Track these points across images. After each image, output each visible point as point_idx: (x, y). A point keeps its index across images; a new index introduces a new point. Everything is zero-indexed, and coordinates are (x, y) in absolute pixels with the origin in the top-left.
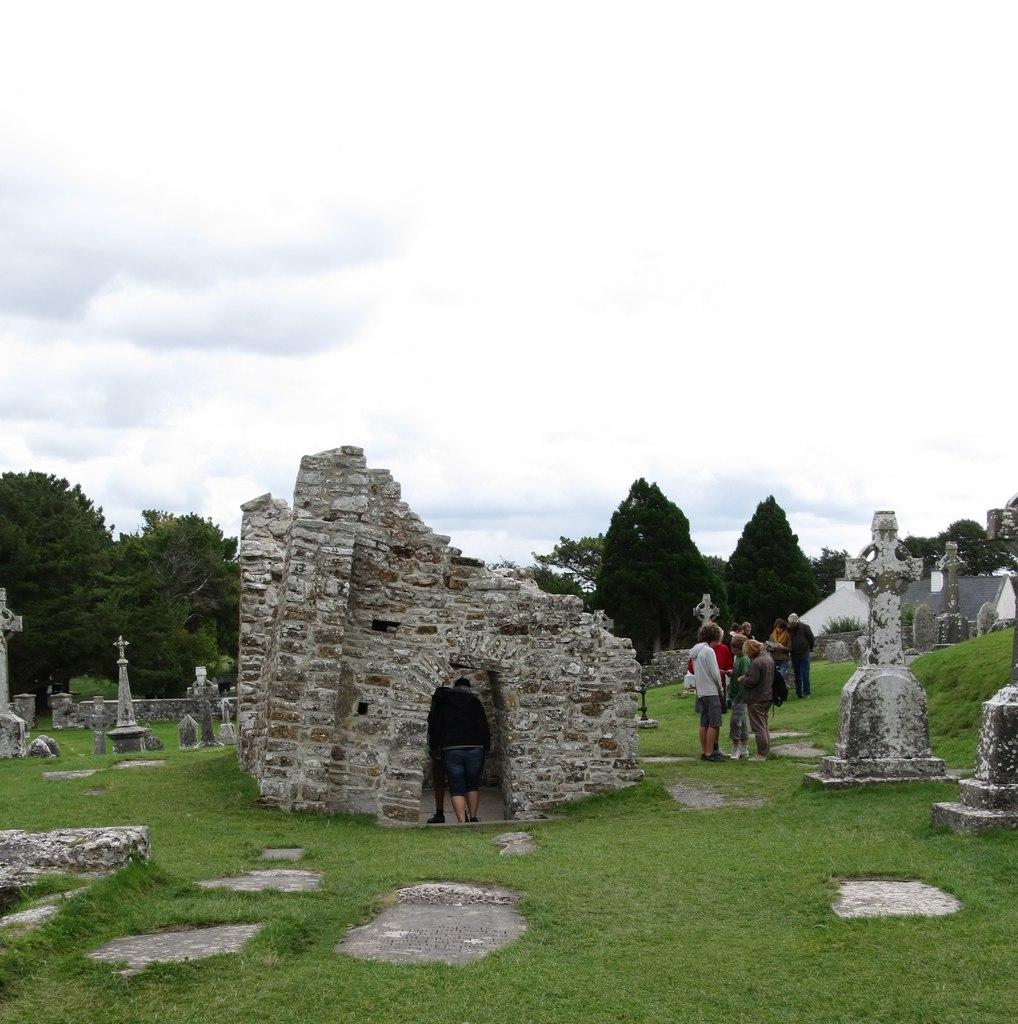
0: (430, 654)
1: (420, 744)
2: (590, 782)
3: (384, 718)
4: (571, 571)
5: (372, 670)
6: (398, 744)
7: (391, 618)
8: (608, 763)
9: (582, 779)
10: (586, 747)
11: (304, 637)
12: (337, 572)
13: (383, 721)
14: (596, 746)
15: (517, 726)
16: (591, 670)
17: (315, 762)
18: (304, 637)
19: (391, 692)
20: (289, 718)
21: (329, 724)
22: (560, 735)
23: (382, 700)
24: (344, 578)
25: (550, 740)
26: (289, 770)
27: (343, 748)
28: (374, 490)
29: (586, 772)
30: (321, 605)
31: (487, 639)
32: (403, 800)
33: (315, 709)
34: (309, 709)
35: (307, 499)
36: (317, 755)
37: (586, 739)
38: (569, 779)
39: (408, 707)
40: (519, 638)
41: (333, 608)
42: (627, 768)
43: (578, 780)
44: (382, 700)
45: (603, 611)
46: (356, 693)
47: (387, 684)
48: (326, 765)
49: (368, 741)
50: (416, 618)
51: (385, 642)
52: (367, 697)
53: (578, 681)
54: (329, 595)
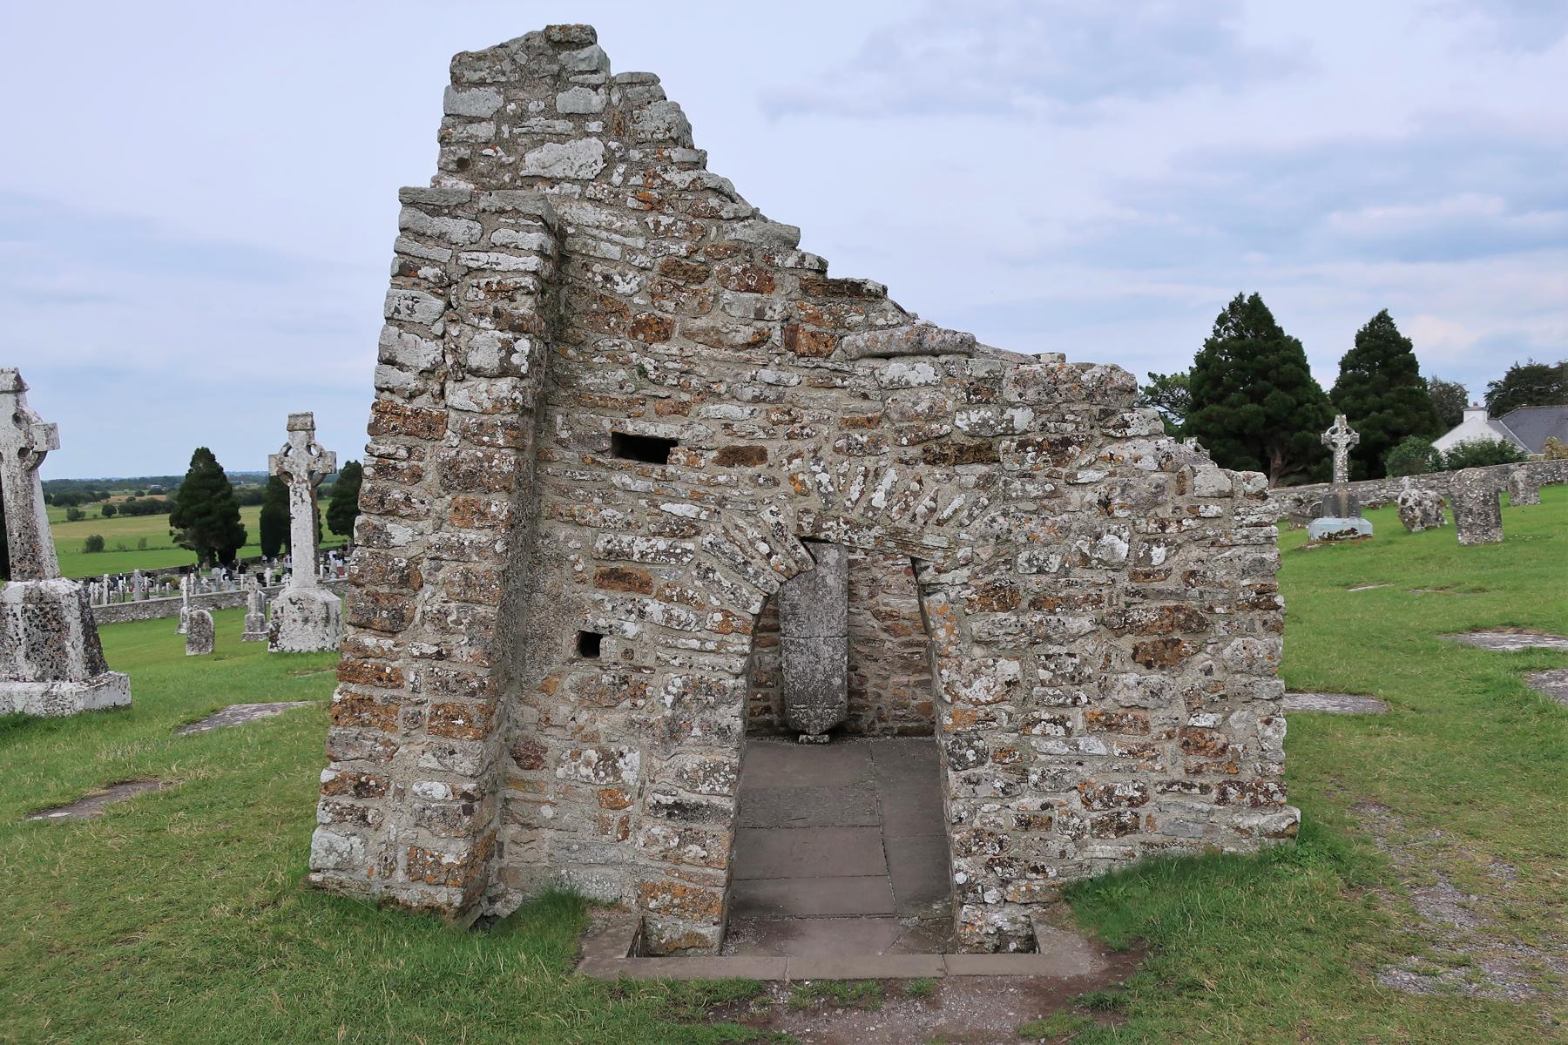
0: (748, 513)
1: (723, 732)
2: (1156, 838)
3: (639, 669)
4: (1164, 410)
5: (610, 553)
6: (674, 732)
7: (660, 430)
8: (1205, 789)
9: (1135, 828)
10: (1145, 747)
11: (417, 476)
12: (497, 314)
13: (635, 677)
14: (1172, 746)
15: (963, 692)
16: (1158, 553)
17: (439, 790)
18: (417, 476)
19: (655, 608)
20: (379, 677)
21: (473, 694)
22: (1077, 720)
23: (631, 628)
24: (513, 328)
25: (1050, 729)
26: (373, 806)
27: (543, 740)
28: (618, 125)
29: (1143, 811)
30: (458, 396)
31: (891, 476)
32: (684, 868)
33: (439, 656)
34: (423, 656)
35: (464, 152)
36: (445, 774)
37: (1146, 728)
38: (1101, 828)
39: (695, 644)
40: (971, 473)
41: (488, 405)
42: (1255, 804)
43: (1122, 829)
44: (631, 628)
45: (1194, 439)
46: (575, 608)
47: (644, 586)
48: (465, 795)
49: (606, 722)
50: (716, 427)
51: (640, 485)
52: (596, 620)
53: (1124, 581)
54: (477, 372)
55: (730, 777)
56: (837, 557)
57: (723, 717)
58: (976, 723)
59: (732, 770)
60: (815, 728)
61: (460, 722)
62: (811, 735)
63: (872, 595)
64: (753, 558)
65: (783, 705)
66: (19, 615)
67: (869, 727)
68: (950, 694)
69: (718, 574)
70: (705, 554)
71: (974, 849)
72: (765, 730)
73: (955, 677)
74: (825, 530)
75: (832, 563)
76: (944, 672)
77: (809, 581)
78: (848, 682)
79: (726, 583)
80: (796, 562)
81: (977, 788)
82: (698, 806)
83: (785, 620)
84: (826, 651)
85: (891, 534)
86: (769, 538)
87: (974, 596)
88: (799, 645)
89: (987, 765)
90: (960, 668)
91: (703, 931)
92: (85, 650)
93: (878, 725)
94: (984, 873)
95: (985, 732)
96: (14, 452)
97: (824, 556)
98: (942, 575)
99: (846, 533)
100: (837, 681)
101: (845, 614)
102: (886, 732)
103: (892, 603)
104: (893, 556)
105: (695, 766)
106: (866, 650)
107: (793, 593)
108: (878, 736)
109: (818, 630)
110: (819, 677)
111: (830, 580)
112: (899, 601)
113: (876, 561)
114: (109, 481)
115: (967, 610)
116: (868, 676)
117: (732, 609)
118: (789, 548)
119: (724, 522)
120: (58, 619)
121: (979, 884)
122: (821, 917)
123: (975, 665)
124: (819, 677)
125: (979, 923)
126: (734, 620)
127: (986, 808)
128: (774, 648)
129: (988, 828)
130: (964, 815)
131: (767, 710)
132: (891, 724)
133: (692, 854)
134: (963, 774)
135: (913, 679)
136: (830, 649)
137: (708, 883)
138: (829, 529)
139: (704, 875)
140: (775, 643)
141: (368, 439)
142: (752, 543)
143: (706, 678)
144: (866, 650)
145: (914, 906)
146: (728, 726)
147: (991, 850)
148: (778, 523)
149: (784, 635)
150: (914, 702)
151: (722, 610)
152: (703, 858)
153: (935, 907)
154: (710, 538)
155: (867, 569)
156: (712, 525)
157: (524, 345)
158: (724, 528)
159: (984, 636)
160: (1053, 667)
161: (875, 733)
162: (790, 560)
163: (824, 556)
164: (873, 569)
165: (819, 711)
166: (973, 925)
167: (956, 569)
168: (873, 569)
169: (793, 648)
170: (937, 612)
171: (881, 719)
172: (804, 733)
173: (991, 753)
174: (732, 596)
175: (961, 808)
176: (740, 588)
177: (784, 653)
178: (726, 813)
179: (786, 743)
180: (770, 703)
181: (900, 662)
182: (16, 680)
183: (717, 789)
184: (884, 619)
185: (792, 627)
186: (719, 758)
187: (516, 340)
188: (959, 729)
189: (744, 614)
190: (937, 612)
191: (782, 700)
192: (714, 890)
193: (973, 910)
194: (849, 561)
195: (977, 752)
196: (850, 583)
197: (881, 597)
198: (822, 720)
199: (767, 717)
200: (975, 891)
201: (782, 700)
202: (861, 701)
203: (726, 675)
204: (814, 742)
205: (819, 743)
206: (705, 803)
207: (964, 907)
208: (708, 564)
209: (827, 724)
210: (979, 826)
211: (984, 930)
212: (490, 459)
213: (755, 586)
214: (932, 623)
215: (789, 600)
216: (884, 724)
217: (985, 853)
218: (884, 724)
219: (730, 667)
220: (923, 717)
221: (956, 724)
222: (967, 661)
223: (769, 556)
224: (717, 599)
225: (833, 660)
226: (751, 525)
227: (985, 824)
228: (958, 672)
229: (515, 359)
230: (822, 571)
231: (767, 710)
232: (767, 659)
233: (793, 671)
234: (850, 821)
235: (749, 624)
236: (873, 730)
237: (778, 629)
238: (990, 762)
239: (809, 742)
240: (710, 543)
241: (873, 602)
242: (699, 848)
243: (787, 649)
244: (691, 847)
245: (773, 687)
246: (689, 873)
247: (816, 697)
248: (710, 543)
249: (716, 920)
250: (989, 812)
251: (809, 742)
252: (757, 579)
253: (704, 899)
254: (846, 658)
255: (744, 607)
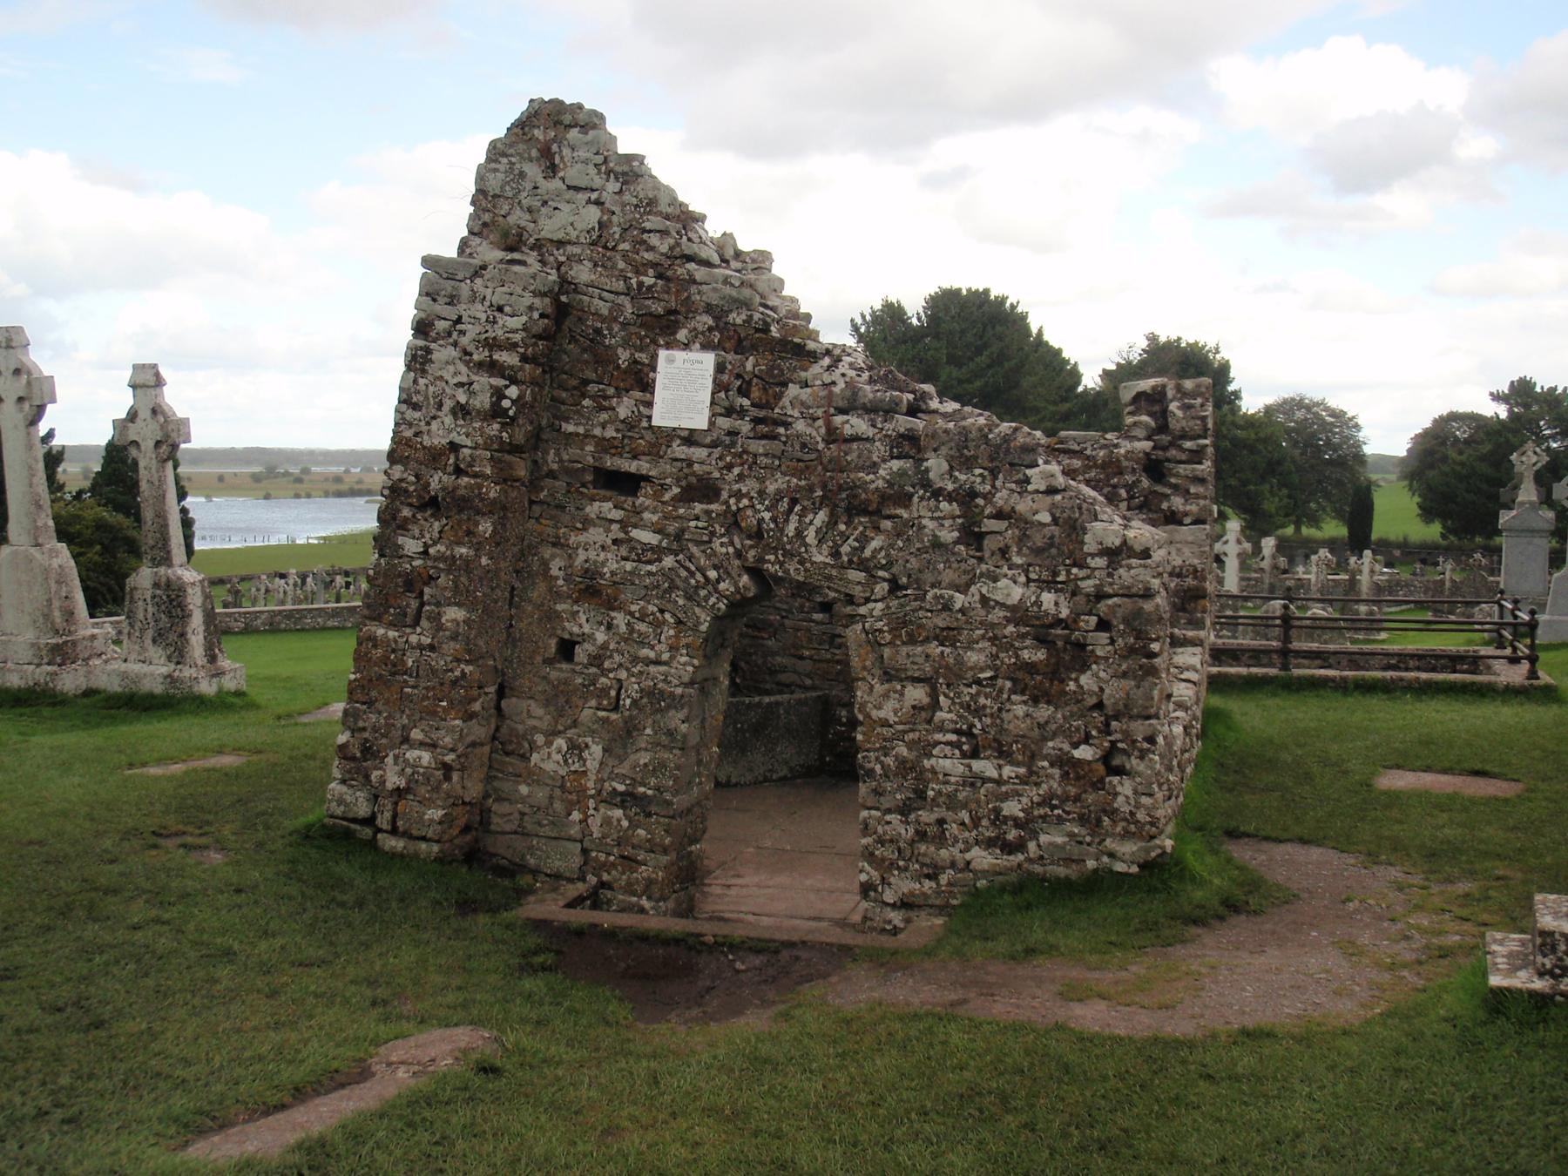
19: (620, 620)
61: (445, 704)
66: (149, 600)
92: (205, 638)
96: (151, 444)
114: (311, 453)
120: (182, 606)
141: (387, 465)
147: (1334, 986)
157: (513, 392)
160: (952, 695)
182: (144, 662)
187: (507, 387)
212: (480, 487)
229: (506, 403)
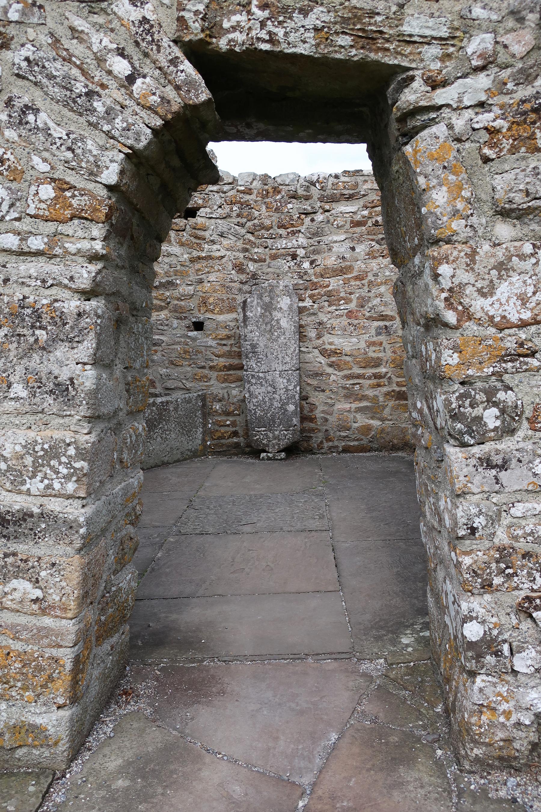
55: (77, 465)
56: (289, 303)
57: (61, 364)
58: (502, 359)
59: (81, 454)
60: (274, 447)
62: (271, 453)
63: (319, 337)
64: (103, 86)
65: (248, 429)
67: (318, 446)
68: (455, 310)
69: (43, 116)
70: (20, 82)
71: (497, 581)
72: (234, 451)
73: (464, 277)
74: (228, 31)
75: (285, 308)
76: (444, 269)
77: (266, 324)
78: (301, 408)
79: (58, 132)
80: (178, 88)
81: (503, 475)
82: (26, 515)
83: (247, 357)
84: (281, 383)
85: (345, 20)
86: (130, 49)
87: (499, 123)
88: (259, 378)
89: (520, 434)
90: (474, 261)
91: (39, 720)
93: (326, 445)
94: (515, 621)
95: (517, 377)
97: (278, 302)
98: (439, 91)
99: (263, 25)
100: (291, 408)
101: (297, 351)
102: (332, 450)
103: (336, 342)
104: (336, 302)
105: (18, 448)
106: (314, 382)
107: (252, 335)
108: (326, 453)
109: (274, 365)
110: (276, 404)
111: (284, 323)
112: (341, 340)
113: (322, 307)
115: (486, 151)
116: (317, 404)
117: (71, 178)
118: (164, 63)
119: (50, 23)
121: (505, 641)
122: (253, 658)
123: (500, 253)
124: (276, 404)
125: (505, 706)
126: (74, 196)
127: (518, 510)
128: (239, 383)
129: (522, 545)
130: (479, 522)
131: (235, 434)
132: (336, 443)
133: (17, 595)
134: (476, 450)
135: (354, 406)
136: (285, 381)
137: (46, 641)
138: (234, 28)
139: (40, 629)
140: (240, 379)
142: (100, 60)
143: (31, 300)
144: (314, 382)
145: (378, 638)
146: (71, 379)
148: (145, 20)
149: (246, 371)
150: (356, 425)
151: (53, 180)
152: (36, 601)
153: (405, 640)
154: (28, 51)
155: (314, 314)
156: (30, 30)
158: (52, 35)
159: (519, 198)
161: (323, 451)
162: (169, 88)
163: (278, 302)
164: (320, 314)
165: (277, 433)
166: (494, 709)
167: (465, 76)
168: (320, 314)
169: (254, 381)
170: (432, 158)
171: (328, 440)
172: (265, 451)
173: (528, 413)
174: (69, 155)
175: (474, 510)
176: (82, 139)
177: (247, 386)
178: (72, 525)
179: (250, 460)
180: (237, 428)
181: (342, 392)
183: (57, 486)
184: (329, 356)
185: (253, 363)
186: (57, 435)
188: (470, 372)
189: (91, 186)
190: (432, 158)
191: (247, 426)
192: (55, 652)
193: (494, 685)
194: (299, 307)
195: (503, 411)
196: (301, 326)
197: (327, 338)
198: (279, 440)
199: (235, 440)
200: (498, 654)
201: (247, 426)
202: (312, 425)
203: (67, 294)
204: (273, 459)
205: (277, 460)
206: (36, 510)
207: (479, 679)
208: (26, 100)
209: (283, 443)
210: (506, 541)
211: (514, 719)
213: (109, 135)
214: (421, 180)
215: (250, 340)
216: (330, 444)
217: (517, 588)
218: (330, 444)
219: (72, 279)
220: (363, 437)
221: (464, 364)
222: (486, 247)
223: (131, 79)
224: (45, 160)
225: (287, 390)
226: (99, 27)
227: (516, 538)
228: (470, 267)
230: (277, 315)
231: (235, 434)
232: (234, 392)
233: (255, 400)
234: (299, 526)
235: (100, 202)
236: (322, 448)
237: (241, 367)
238: (524, 430)
239: (269, 459)
240: (27, 59)
241: (320, 341)
242: (27, 586)
243: (249, 382)
244: (15, 583)
245: (239, 415)
246: (14, 626)
247: (274, 422)
248: (27, 59)
249: (61, 701)
250: (524, 517)
251: (269, 459)
252: (110, 121)
253: (39, 669)
254: (298, 388)
255: (91, 174)
